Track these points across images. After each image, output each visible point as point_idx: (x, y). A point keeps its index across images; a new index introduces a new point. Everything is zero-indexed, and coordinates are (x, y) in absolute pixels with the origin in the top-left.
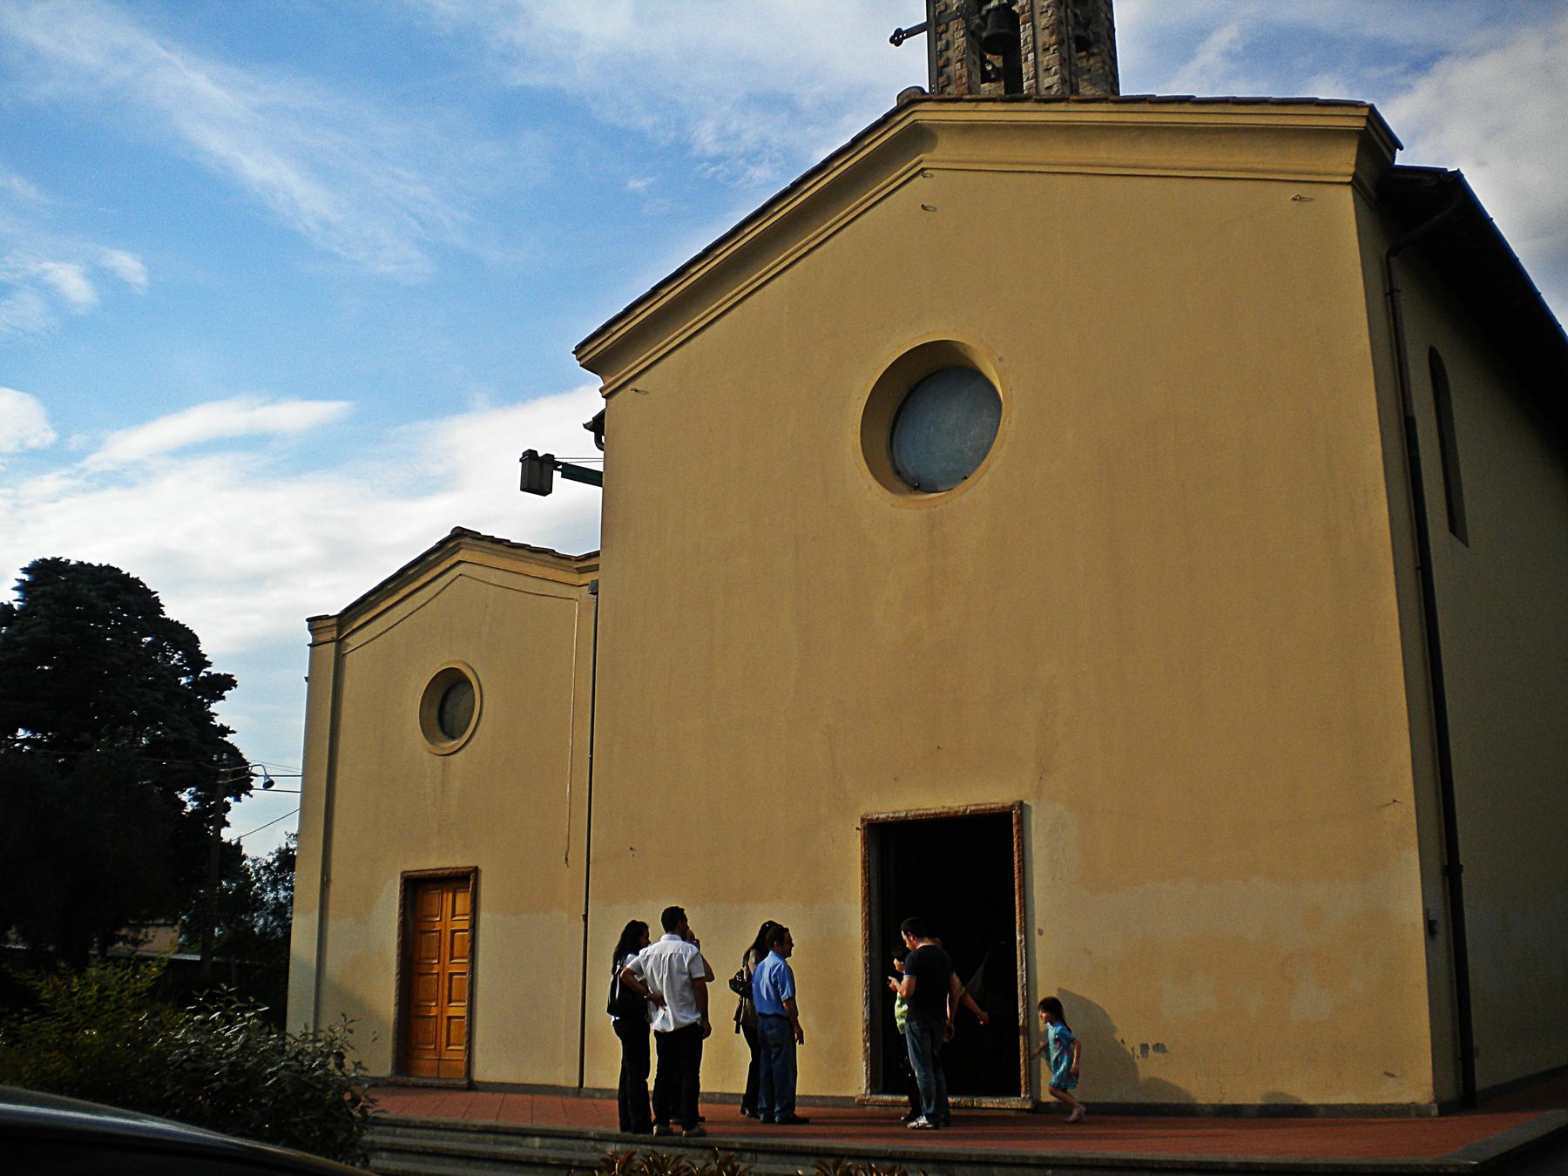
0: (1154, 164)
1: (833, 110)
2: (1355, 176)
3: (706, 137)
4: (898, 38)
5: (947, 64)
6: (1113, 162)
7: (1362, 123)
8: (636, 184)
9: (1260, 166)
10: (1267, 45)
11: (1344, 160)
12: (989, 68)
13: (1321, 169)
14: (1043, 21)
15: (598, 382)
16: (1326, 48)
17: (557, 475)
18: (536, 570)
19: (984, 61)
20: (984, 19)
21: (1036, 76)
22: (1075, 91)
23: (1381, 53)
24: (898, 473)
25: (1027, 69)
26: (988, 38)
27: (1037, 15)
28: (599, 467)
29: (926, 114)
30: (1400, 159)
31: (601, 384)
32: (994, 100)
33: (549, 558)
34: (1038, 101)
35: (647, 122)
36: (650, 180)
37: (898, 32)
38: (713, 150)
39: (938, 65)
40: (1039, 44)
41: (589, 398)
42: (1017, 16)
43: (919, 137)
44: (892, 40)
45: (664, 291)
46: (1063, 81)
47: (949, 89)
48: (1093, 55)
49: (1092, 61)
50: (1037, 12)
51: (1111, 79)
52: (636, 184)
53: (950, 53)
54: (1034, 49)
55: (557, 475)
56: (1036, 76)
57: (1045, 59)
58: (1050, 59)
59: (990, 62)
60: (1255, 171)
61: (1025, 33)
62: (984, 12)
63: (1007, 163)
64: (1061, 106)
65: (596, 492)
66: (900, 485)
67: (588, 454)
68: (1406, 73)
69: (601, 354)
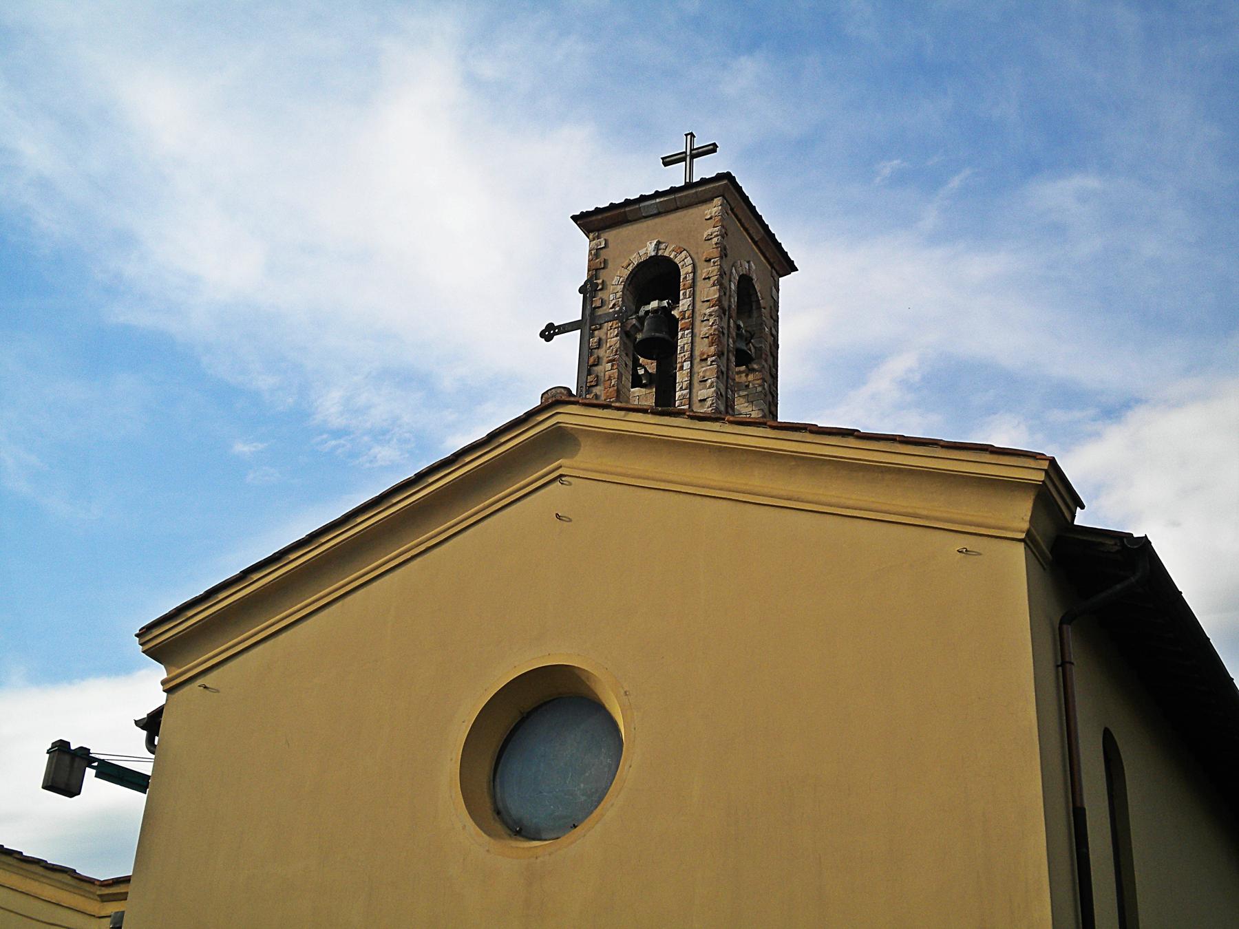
0: (810, 498)
1: (473, 397)
2: (1028, 533)
3: (330, 406)
4: (549, 333)
5: (598, 362)
6: (766, 490)
7: (1041, 477)
8: (242, 448)
9: (925, 512)
10: (948, 379)
11: (1019, 514)
12: (641, 372)
13: (992, 522)
14: (703, 329)
15: (160, 672)
16: (1008, 387)
17: (90, 773)
18: (49, 892)
19: (636, 364)
20: (641, 320)
21: (690, 386)
22: (730, 406)
23: (1068, 395)
24: (499, 813)
25: (681, 378)
26: (641, 341)
27: (697, 323)
28: (146, 768)
29: (570, 417)
30: (1081, 518)
31: (164, 675)
32: (644, 411)
33: (67, 878)
34: (691, 417)
35: (264, 382)
36: (260, 446)
37: (550, 326)
38: (337, 422)
39: (588, 363)
40: (697, 353)
41: (147, 687)
42: (677, 321)
43: (561, 439)
44: (542, 335)
45: (255, 576)
46: (719, 395)
47: (597, 390)
48: (753, 370)
49: (751, 377)
50: (698, 319)
51: (769, 398)
52: (242, 448)
53: (601, 352)
54: (691, 358)
55: (90, 773)
56: (690, 386)
57: (701, 370)
58: (707, 370)
59: (643, 367)
60: (920, 517)
61: (683, 341)
62: (642, 313)
63: (653, 479)
64: (716, 426)
65: (137, 800)
66: (499, 827)
67: (132, 751)
68: (1094, 420)
69: (168, 641)
